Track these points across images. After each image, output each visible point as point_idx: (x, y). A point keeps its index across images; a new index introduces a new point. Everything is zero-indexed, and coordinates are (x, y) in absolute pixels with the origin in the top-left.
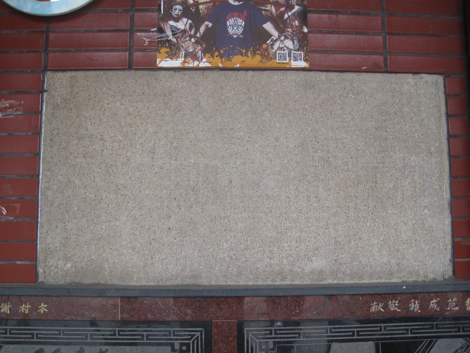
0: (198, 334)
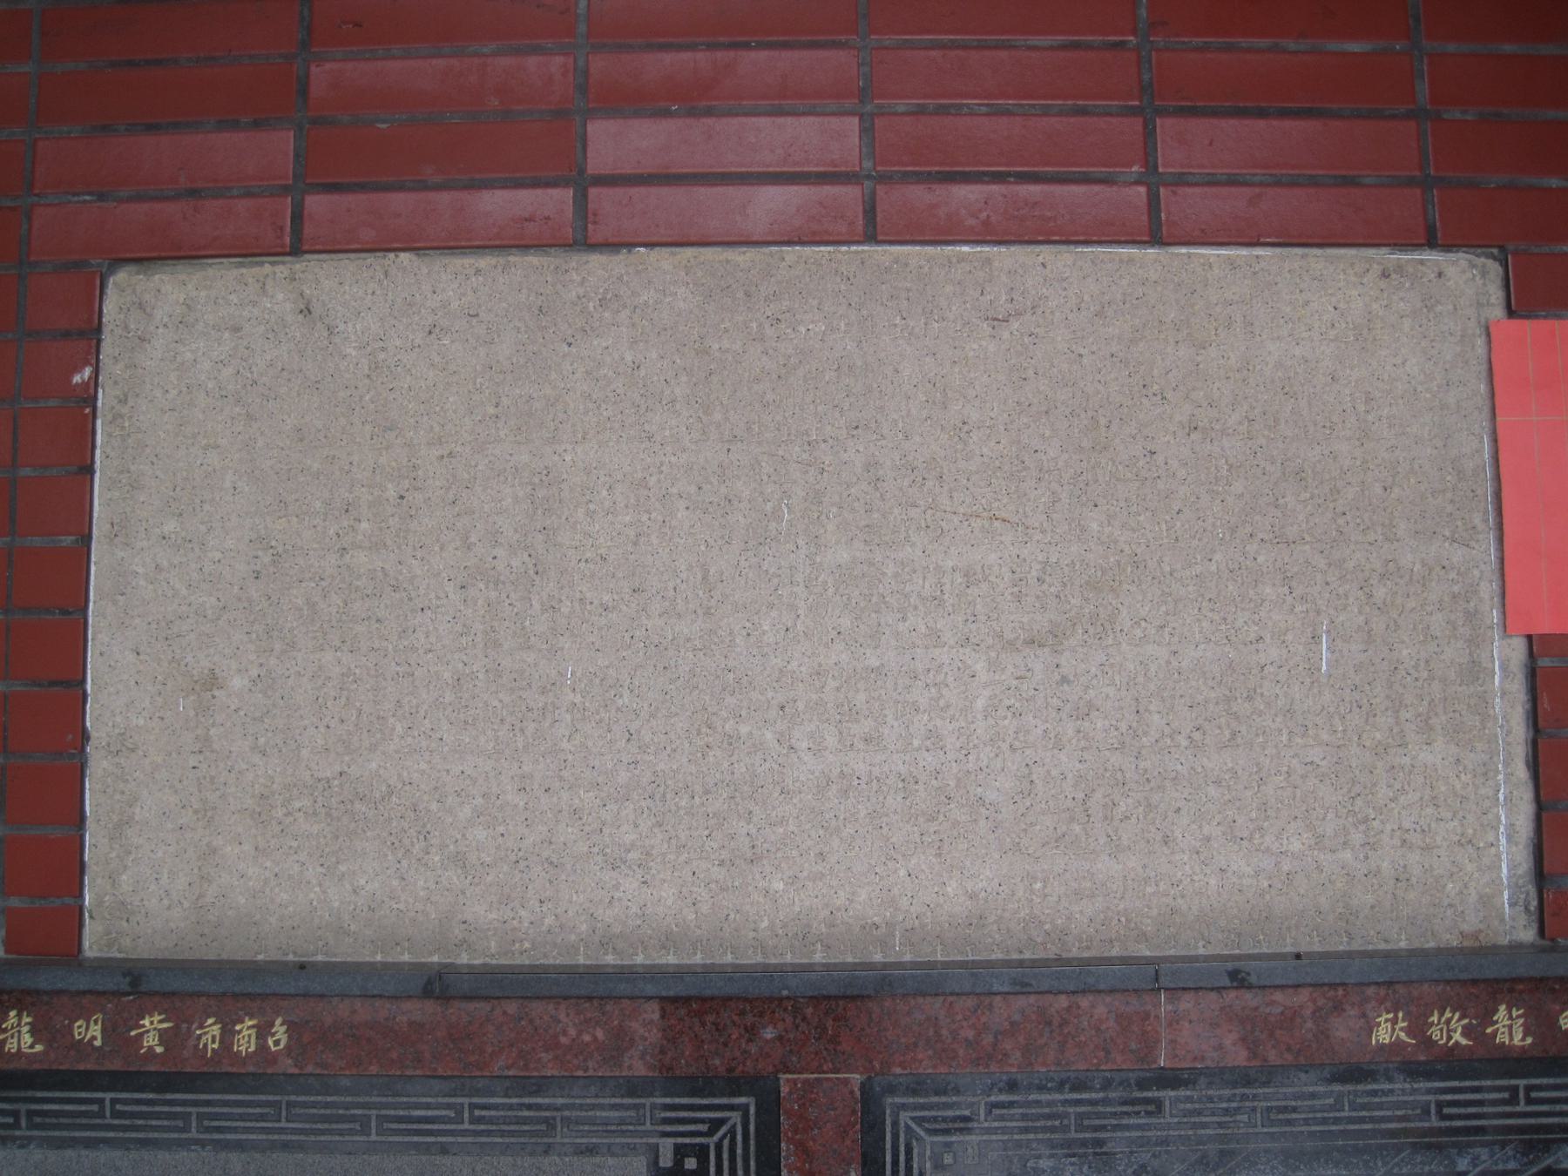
0: (736, 1117)
